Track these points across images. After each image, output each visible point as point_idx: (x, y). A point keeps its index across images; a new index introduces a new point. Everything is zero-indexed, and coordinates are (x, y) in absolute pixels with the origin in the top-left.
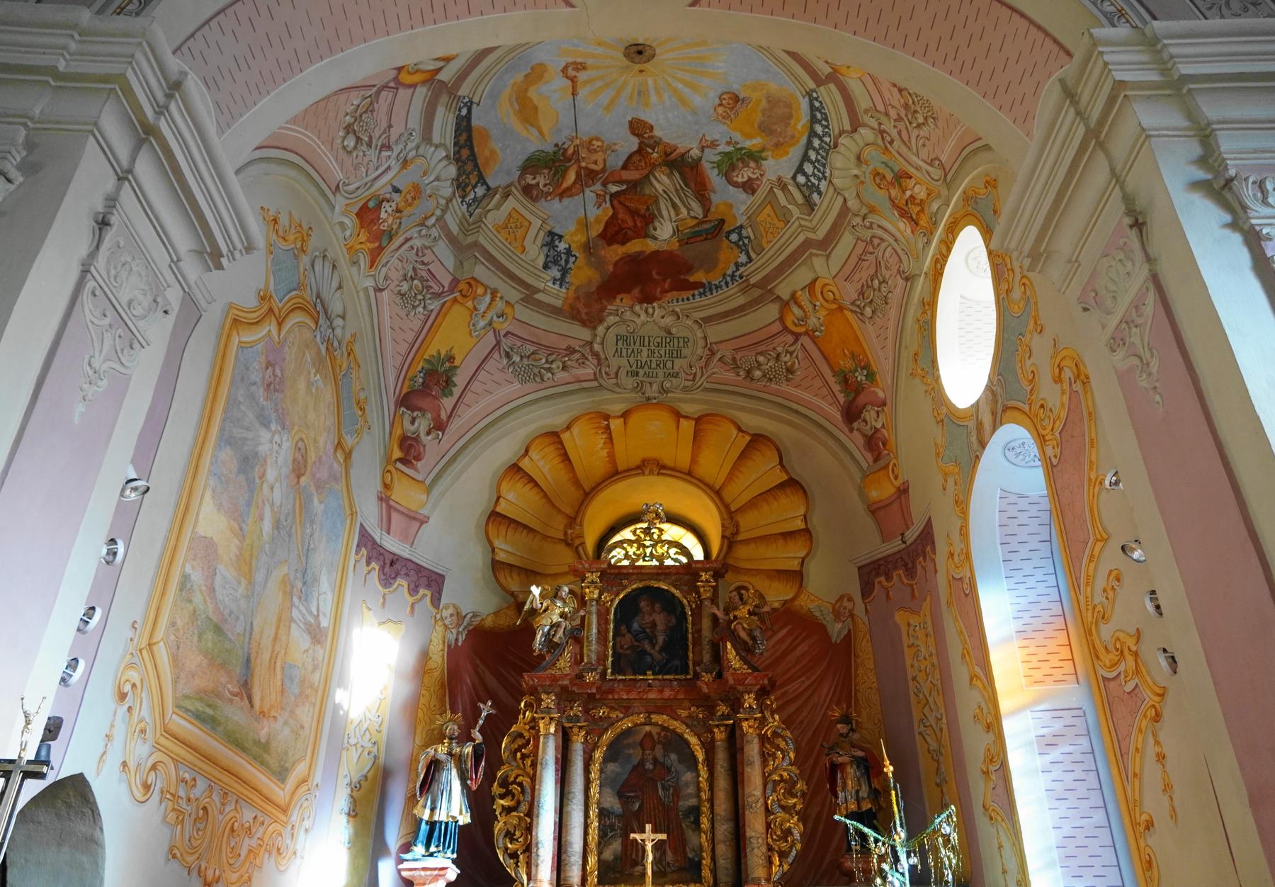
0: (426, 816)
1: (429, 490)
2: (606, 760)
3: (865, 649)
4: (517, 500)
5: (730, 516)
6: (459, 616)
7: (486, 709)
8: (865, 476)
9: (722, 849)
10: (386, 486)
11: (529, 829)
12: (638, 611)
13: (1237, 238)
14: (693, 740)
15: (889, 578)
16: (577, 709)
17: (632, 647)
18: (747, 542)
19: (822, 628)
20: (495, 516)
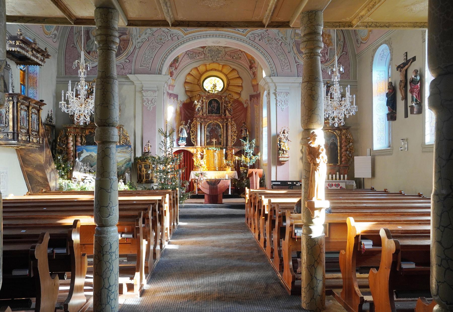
1: (175, 80)
3: (249, 110)
4: (189, 79)
5: (228, 80)
7: (189, 121)
9: (224, 141)
11: (196, 138)
16: (203, 120)
20: (186, 82)
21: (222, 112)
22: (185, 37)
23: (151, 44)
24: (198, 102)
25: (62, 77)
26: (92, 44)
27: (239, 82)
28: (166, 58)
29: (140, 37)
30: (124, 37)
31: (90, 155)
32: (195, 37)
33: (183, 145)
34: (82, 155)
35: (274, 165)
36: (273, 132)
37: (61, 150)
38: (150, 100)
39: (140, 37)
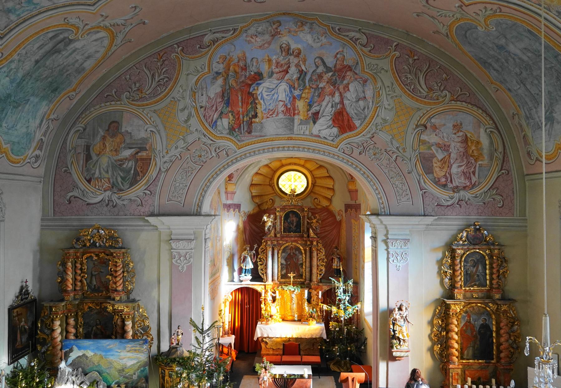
1: (236, 185)
2: (282, 253)
3: (344, 225)
4: (257, 180)
5: (314, 177)
6: (245, 213)
7: (256, 246)
8: (349, 182)
10: (226, 189)
11: (266, 269)
14: (301, 248)
15: (351, 210)
18: (318, 186)
20: (252, 185)
21: (304, 231)
22: (239, 151)
23: (185, 165)
24: (269, 217)
26: (93, 167)
27: (329, 183)
28: (208, 187)
29: (167, 153)
30: (144, 154)
31: (84, 355)
32: (254, 152)
33: (247, 281)
34: (71, 354)
35: (383, 359)
36: (383, 305)
37: (43, 338)
38: (183, 255)
39: (167, 153)
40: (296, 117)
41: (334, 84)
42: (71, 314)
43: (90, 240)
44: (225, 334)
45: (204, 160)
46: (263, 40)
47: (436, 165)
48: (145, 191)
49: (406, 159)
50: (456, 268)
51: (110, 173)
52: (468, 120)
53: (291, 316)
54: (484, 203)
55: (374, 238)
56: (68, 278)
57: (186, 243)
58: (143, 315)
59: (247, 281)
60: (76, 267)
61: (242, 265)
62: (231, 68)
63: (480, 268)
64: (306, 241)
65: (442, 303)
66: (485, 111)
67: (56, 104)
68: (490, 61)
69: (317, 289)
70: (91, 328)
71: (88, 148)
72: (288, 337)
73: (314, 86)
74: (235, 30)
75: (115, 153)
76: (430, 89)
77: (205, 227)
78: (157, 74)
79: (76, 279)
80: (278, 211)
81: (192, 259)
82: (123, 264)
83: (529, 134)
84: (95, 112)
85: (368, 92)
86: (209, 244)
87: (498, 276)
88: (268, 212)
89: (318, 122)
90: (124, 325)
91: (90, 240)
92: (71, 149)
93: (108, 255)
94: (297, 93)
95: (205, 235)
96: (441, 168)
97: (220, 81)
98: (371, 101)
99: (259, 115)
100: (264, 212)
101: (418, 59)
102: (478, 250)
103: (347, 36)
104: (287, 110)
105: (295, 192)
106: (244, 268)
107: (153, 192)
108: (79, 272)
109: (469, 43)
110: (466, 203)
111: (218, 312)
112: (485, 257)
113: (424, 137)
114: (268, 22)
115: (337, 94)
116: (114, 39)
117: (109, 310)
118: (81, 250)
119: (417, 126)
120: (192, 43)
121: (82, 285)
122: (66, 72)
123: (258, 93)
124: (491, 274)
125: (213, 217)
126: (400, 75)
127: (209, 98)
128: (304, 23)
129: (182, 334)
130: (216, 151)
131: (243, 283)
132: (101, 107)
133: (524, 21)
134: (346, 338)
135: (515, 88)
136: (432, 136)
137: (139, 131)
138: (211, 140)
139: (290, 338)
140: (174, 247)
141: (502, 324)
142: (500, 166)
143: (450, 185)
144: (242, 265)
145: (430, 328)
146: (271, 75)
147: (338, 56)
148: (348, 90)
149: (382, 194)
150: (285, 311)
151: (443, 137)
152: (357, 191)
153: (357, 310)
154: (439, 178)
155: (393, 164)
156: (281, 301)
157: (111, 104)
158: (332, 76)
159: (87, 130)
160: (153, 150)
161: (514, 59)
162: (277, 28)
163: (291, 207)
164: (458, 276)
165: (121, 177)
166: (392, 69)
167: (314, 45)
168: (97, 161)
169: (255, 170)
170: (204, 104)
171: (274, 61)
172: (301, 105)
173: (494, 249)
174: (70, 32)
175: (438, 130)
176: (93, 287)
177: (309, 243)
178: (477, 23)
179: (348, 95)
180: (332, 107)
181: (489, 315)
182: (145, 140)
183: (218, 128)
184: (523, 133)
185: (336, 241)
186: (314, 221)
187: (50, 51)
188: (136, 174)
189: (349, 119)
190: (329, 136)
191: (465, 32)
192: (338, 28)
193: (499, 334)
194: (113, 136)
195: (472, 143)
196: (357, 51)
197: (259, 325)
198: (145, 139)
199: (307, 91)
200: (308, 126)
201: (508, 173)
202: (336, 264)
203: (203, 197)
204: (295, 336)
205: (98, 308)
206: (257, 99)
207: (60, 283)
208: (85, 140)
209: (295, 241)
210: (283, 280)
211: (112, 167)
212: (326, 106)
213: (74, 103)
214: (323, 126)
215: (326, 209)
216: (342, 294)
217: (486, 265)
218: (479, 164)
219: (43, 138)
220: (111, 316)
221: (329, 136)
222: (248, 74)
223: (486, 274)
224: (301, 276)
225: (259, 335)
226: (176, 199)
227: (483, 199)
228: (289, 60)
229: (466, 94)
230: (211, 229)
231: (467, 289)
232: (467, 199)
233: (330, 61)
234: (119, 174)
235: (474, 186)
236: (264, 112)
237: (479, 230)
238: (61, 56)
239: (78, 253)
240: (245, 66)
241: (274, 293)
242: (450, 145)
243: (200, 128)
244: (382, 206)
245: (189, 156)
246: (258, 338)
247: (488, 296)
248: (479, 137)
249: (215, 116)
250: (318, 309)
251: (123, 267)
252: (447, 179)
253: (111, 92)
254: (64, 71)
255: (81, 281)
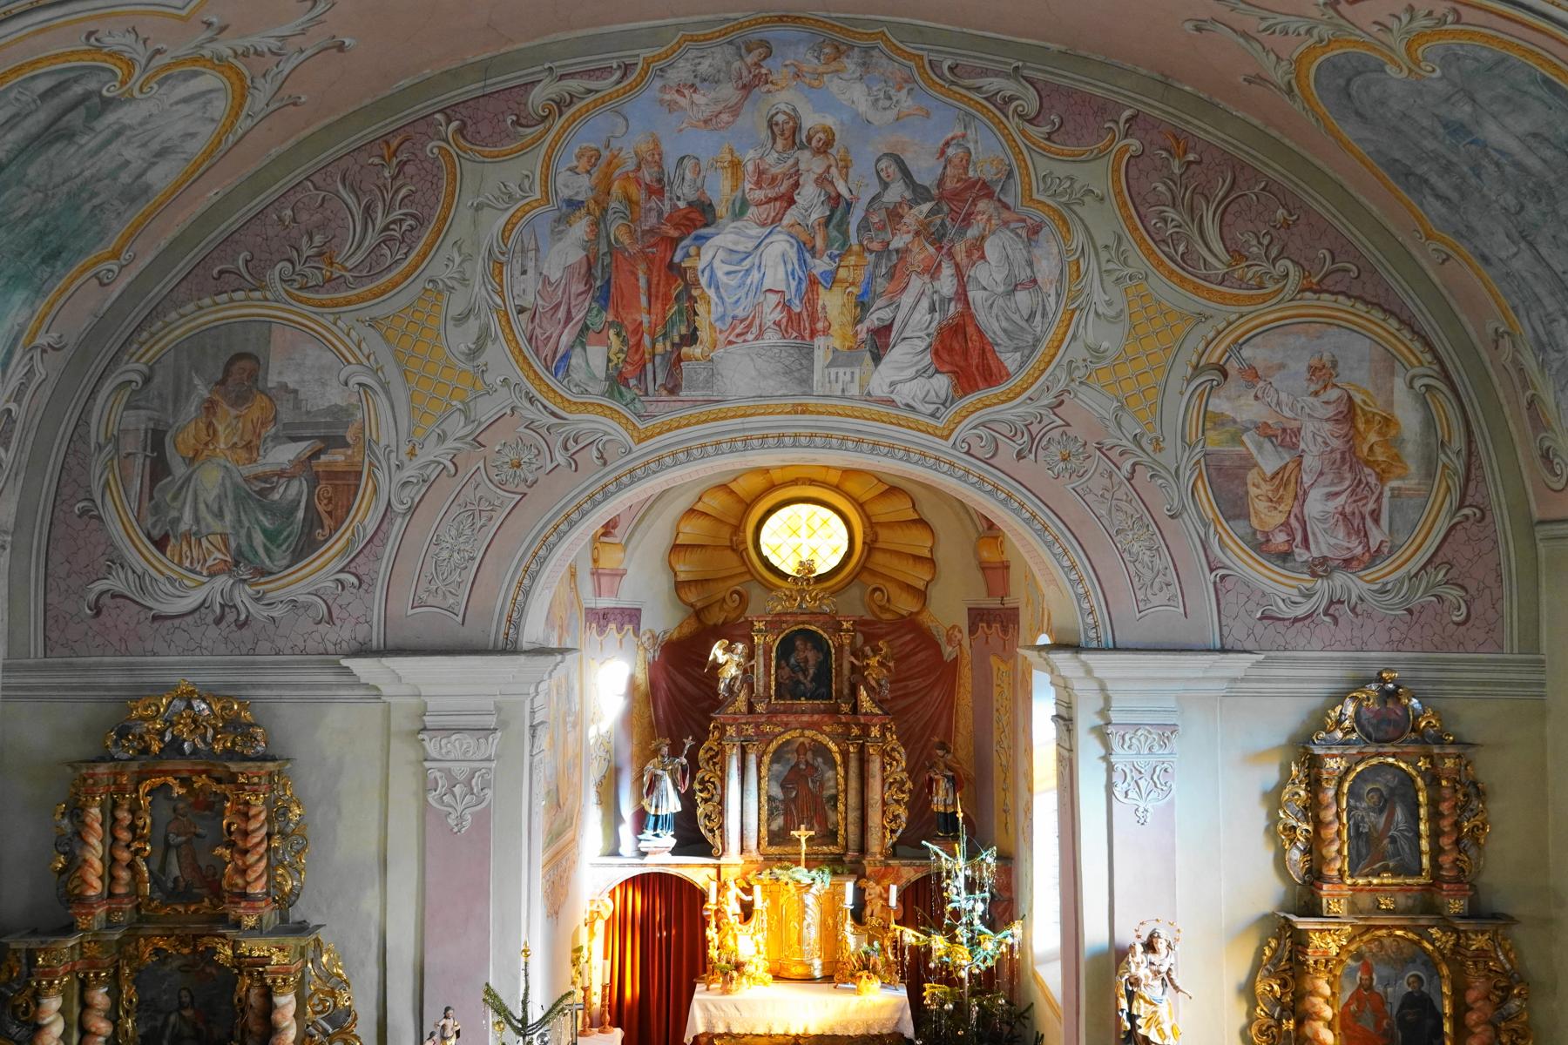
0: (652, 812)
2: (772, 762)
4: (692, 531)
5: (871, 525)
7: (689, 742)
8: (980, 538)
9: (851, 828)
10: (595, 561)
11: (722, 813)
12: (794, 649)
13: (1104, 765)
14: (833, 747)
15: (989, 626)
17: (790, 678)
18: (885, 551)
19: (936, 646)
20: (676, 548)
21: (840, 693)
22: (638, 450)
23: (470, 488)
24: (728, 650)
25: (29, 668)
26: (175, 498)
27: (918, 542)
29: (412, 454)
30: (337, 457)
32: (688, 451)
33: (661, 853)
36: (1095, 934)
38: (461, 778)
39: (412, 454)
40: (820, 341)
41: (937, 240)
42: (97, 975)
43: (161, 733)
44: (591, 1026)
45: (531, 478)
46: (716, 102)
47: (1257, 492)
48: (342, 576)
49: (1163, 473)
50: (1322, 815)
51: (228, 517)
52: (1357, 352)
53: (802, 963)
54: (1410, 611)
55: (1065, 721)
56: (88, 856)
57: (472, 742)
58: (330, 975)
59: (661, 853)
60: (115, 820)
61: (645, 802)
62: (616, 189)
63: (1399, 815)
64: (847, 725)
65: (1282, 928)
66: (1408, 323)
67: (55, 301)
68: (1422, 169)
69: (883, 876)
70: (161, 1018)
71: (157, 439)
72: (793, 1032)
73: (875, 246)
74: (627, 69)
75: (244, 454)
76: (1237, 255)
77: (532, 690)
78: (380, 205)
79: (114, 860)
80: (760, 631)
81: (489, 793)
82: (269, 811)
83: (1549, 398)
84: (182, 325)
85: (1044, 263)
86: (543, 740)
87: (1457, 842)
88: (733, 631)
89: (886, 359)
90: (269, 1008)
91: (161, 733)
92: (102, 440)
93: (219, 781)
94: (821, 265)
95: (533, 712)
96: (1274, 502)
97: (580, 228)
98: (1053, 292)
99: (703, 334)
100: (716, 633)
101: (1199, 163)
102: (1391, 760)
103: (978, 89)
104: (790, 319)
105: (811, 571)
106: (652, 812)
107: (364, 578)
108: (125, 836)
109: (1358, 114)
110: (1353, 610)
111: (569, 956)
112: (1413, 781)
113: (1219, 404)
114: (730, 43)
115: (947, 271)
116: (243, 97)
117: (220, 958)
118: (134, 766)
119: (1197, 370)
120: (491, 110)
121: (133, 878)
122: (90, 199)
123: (701, 266)
124: (1435, 835)
125: (559, 658)
126: (1142, 210)
127: (546, 281)
128: (843, 48)
129: (458, 1033)
130: (566, 449)
131: (647, 860)
132: (200, 308)
133: (1493, 37)
134: (978, 1034)
135: (1503, 255)
136: (1242, 401)
137: (324, 384)
138: (554, 414)
139: (797, 1037)
140: (434, 754)
141: (1471, 996)
142: (1456, 495)
143: (1301, 555)
144: (645, 802)
145: (1244, 1007)
146: (740, 209)
147: (950, 151)
148: (983, 257)
149: (1090, 582)
150: (781, 950)
151: (1278, 404)
152: (1006, 567)
153: (1012, 946)
154: (1266, 534)
155: (1123, 489)
156: (770, 918)
157: (232, 300)
158: (931, 212)
159: (157, 380)
160: (370, 445)
161: (1497, 164)
162: (758, 65)
163: (801, 618)
164: (1332, 842)
165: (265, 531)
166: (1119, 193)
167: (877, 118)
168: (188, 479)
169: (683, 504)
170: (528, 301)
171: (750, 167)
172: (833, 303)
173: (1442, 757)
174: (105, 76)
175: (1261, 384)
176: (170, 885)
177: (855, 731)
178: (1382, 54)
179: (980, 273)
180: (932, 310)
181: (1430, 964)
182: (340, 415)
183: (574, 376)
184: (1529, 393)
185: (943, 724)
186: (874, 661)
187: (39, 136)
188: (313, 520)
189: (986, 349)
190: (924, 401)
191: (1347, 80)
192: (949, 62)
193: (1464, 1026)
194: (241, 399)
195: (1367, 422)
196: (1008, 136)
197: (701, 996)
198: (342, 409)
199: (852, 260)
200: (857, 371)
201: (1483, 517)
202: (941, 799)
203: (527, 594)
204: (814, 1030)
205: (186, 951)
206: (697, 284)
207: (61, 872)
208: (149, 413)
209: (810, 726)
210: (774, 850)
211: (235, 498)
212: (914, 308)
213: (115, 295)
214: (902, 369)
215: (910, 624)
216: (964, 894)
217: (1418, 805)
218: (1392, 489)
219: (13, 406)
220: (227, 979)
221: (924, 401)
222: (667, 208)
223: (1418, 836)
224: (830, 836)
225: (701, 1029)
226: (438, 601)
227: (1406, 599)
228: (797, 163)
229: (1348, 271)
230: (548, 694)
231: (1361, 881)
232: (1354, 599)
233: (926, 169)
234: (258, 522)
235: (1375, 556)
236: (718, 325)
237: (1394, 694)
238: (72, 150)
239: (121, 774)
240: (660, 181)
241: (748, 890)
242: (1299, 430)
243: (517, 374)
244: (1090, 620)
245: (481, 464)
246: (696, 1038)
247: (1427, 905)
248: (1390, 403)
249: (564, 338)
250: (887, 943)
251: (269, 820)
252: (1291, 535)
253: (235, 260)
254: (85, 195)
255: (131, 866)
